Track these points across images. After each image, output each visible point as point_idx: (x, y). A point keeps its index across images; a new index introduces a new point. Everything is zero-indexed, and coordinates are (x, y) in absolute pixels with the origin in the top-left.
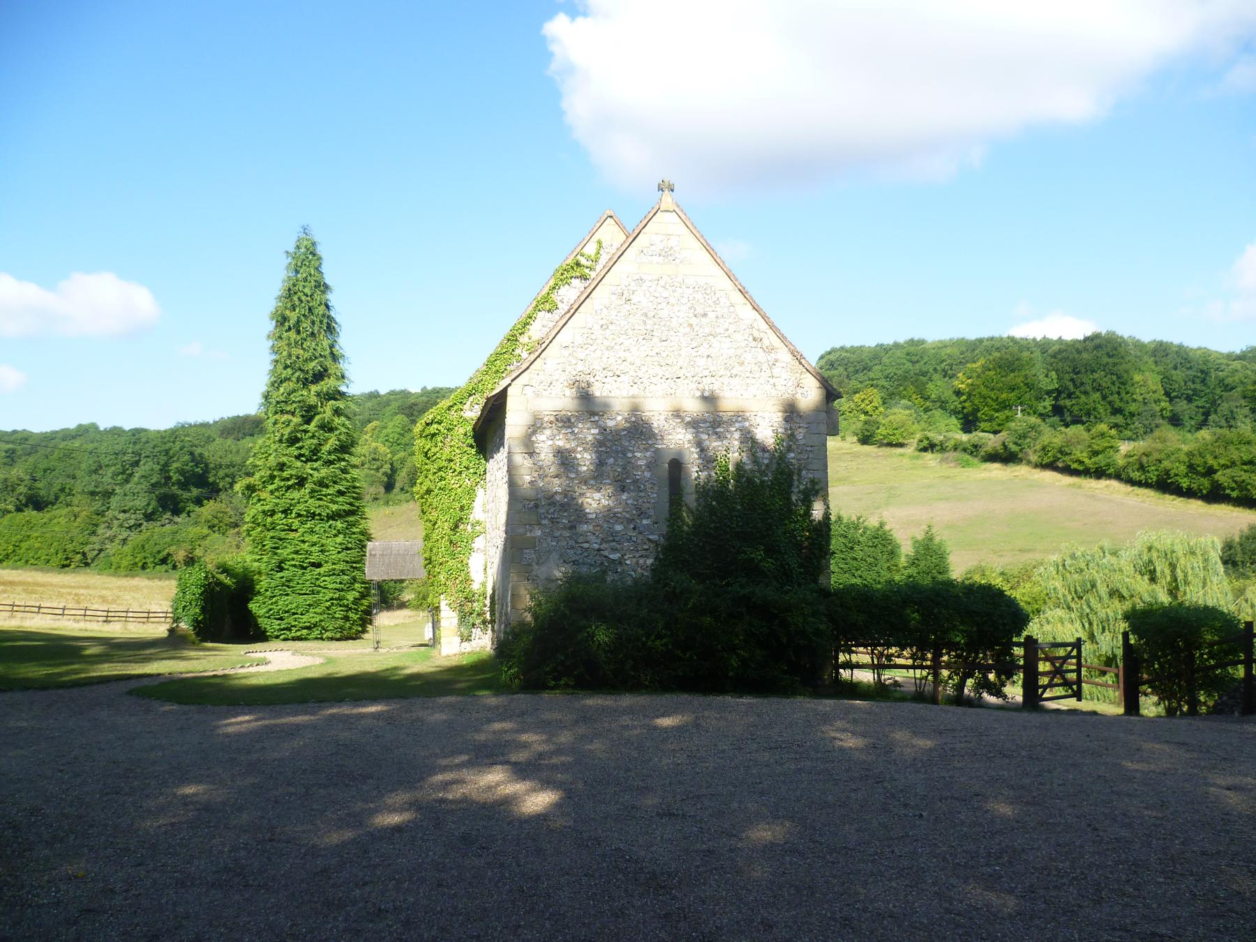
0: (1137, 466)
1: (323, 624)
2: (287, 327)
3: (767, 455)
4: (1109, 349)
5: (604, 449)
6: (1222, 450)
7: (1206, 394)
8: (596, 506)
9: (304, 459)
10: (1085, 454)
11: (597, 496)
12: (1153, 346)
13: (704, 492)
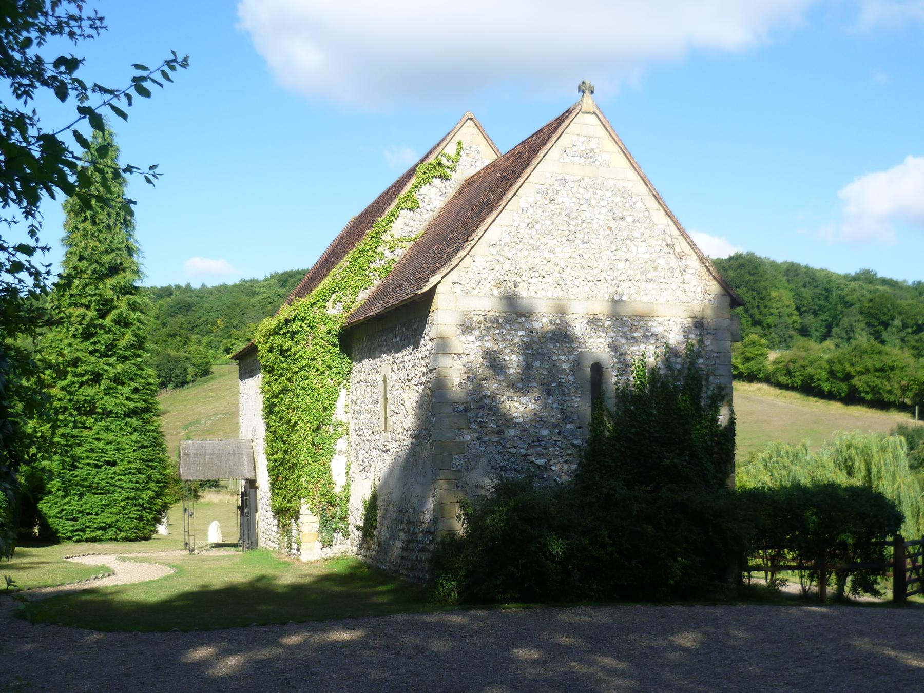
0: (784, 372)
1: (119, 524)
2: (83, 218)
3: (679, 360)
4: (751, 268)
5: (530, 351)
6: (858, 359)
7: (828, 310)
8: (522, 409)
9: (97, 354)
10: (739, 360)
11: (524, 399)
12: (785, 267)
13: (623, 395)
